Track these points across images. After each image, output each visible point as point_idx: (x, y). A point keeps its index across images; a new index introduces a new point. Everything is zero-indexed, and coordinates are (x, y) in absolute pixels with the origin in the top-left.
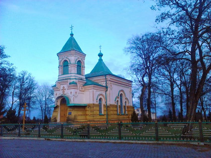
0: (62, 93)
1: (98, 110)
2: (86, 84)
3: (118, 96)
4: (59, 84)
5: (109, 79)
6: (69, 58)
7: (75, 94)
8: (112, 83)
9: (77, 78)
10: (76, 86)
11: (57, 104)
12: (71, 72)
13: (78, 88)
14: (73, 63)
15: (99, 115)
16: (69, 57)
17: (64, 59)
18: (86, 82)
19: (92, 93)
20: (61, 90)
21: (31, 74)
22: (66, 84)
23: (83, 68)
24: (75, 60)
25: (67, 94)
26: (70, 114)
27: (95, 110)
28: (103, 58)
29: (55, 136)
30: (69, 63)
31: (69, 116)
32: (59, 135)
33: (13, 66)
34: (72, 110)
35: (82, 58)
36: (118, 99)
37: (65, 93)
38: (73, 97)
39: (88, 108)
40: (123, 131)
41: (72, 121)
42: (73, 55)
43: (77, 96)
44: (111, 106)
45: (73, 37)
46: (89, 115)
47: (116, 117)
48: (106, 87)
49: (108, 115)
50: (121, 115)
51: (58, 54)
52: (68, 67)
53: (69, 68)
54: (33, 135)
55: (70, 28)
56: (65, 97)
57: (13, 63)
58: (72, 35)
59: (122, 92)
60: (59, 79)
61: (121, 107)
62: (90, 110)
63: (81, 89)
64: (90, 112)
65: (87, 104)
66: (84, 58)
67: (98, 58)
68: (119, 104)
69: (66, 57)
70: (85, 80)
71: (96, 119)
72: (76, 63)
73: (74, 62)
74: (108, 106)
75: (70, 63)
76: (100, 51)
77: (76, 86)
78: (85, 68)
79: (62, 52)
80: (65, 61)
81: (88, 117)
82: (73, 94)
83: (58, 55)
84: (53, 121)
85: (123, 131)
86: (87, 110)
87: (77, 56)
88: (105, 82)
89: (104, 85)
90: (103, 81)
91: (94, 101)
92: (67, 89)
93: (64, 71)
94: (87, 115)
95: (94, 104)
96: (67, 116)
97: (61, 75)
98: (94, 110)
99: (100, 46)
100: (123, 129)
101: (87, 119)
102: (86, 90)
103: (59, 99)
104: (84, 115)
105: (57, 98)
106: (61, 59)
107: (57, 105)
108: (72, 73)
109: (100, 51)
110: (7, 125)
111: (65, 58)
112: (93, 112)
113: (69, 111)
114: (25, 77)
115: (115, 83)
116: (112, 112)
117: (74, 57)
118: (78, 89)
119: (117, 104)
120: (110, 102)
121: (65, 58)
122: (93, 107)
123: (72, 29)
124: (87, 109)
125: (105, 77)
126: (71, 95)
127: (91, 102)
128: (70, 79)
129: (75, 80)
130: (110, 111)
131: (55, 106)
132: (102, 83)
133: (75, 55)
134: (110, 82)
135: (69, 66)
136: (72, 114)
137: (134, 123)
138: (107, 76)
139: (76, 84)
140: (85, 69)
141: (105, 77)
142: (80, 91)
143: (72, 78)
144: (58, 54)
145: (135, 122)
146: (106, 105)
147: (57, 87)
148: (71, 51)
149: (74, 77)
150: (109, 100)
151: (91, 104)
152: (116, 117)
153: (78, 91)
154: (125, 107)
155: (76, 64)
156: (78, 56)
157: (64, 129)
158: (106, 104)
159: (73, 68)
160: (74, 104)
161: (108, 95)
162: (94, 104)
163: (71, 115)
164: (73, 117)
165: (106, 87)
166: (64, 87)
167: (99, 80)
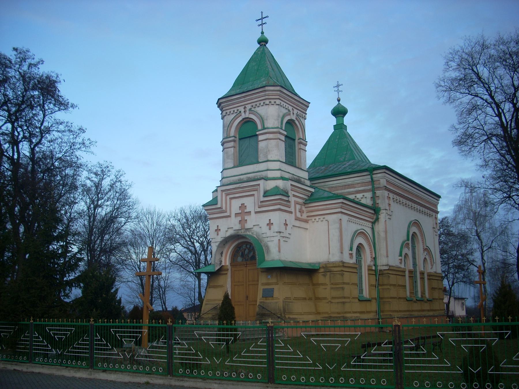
0: (238, 227)
1: (356, 284)
2: (311, 199)
3: (406, 238)
4: (227, 195)
5: (383, 182)
6: (262, 110)
7: (283, 229)
8: (391, 195)
9: (287, 176)
10: (285, 203)
11: (221, 262)
12: (266, 155)
13: (292, 209)
14: (273, 128)
15: (357, 300)
16: (261, 108)
17: (243, 116)
18: (313, 190)
19: (337, 225)
20: (233, 215)
21: (121, 173)
22: (253, 195)
23: (302, 146)
24: (279, 116)
25: (256, 229)
26: (268, 294)
27: (348, 284)
28: (347, 120)
29: (144, 367)
30: (260, 127)
32: (255, 371)
33: (82, 135)
34: (274, 280)
37: (248, 225)
38: (276, 240)
39: (325, 276)
40: (282, 353)
41: (279, 317)
42: (273, 101)
43: (288, 236)
44: (393, 271)
45: (266, 49)
46: (325, 298)
47: (403, 306)
48: (375, 210)
49: (380, 300)
50: (415, 302)
51: (221, 101)
52: (257, 142)
53: (261, 145)
54: (207, 370)
58: (263, 42)
60: (225, 181)
64: (332, 288)
65: (319, 263)
66: (304, 115)
67: (333, 121)
69: (249, 107)
70: (308, 183)
71: (350, 312)
72: (284, 128)
73: (276, 122)
74: (380, 270)
75: (264, 128)
76: (339, 100)
78: (306, 145)
79: (233, 93)
80: (247, 121)
81: (325, 307)
82: (275, 228)
83: (219, 104)
84: (210, 316)
85: (282, 353)
86: (319, 284)
87: (285, 104)
88: (369, 195)
89: (368, 201)
91: (344, 252)
92: (256, 212)
93: (240, 156)
94: (318, 299)
95: (343, 263)
97: (232, 166)
98: (344, 283)
99: (338, 86)
100: (281, 348)
101: (319, 313)
102: (313, 218)
103: (227, 247)
104: (310, 299)
105: (221, 242)
106: (232, 116)
107: (221, 263)
108: (270, 159)
109: (339, 100)
110: (116, 327)
111: (245, 112)
112: (343, 289)
113: (263, 284)
114: (106, 183)
115: (398, 198)
116: (393, 292)
117: (278, 106)
118: (291, 212)
120: (387, 256)
121: (245, 112)
122: (342, 275)
123: (262, 24)
124: (320, 278)
125: (369, 177)
126: (269, 233)
127: (335, 258)
128: (266, 179)
129: (280, 184)
130: (389, 287)
131: (217, 268)
132: (359, 196)
133: (278, 102)
134: (386, 193)
135: (260, 138)
136: (276, 294)
138: (375, 172)
139: (286, 194)
140: (307, 148)
141: (369, 177)
142: (297, 219)
143: (270, 174)
144: (221, 101)
145: (512, 320)
146: (374, 268)
147: (219, 206)
148: (267, 88)
149: (278, 174)
150: (383, 252)
151: (333, 263)
152: (403, 306)
153: (290, 219)
154: (422, 273)
155: (282, 129)
156: (287, 105)
157: (278, 348)
158: (375, 265)
159: (273, 142)
160: (282, 261)
161: (382, 235)
162: (345, 265)
163: (273, 297)
164: (281, 305)
165: (374, 210)
166: (243, 206)
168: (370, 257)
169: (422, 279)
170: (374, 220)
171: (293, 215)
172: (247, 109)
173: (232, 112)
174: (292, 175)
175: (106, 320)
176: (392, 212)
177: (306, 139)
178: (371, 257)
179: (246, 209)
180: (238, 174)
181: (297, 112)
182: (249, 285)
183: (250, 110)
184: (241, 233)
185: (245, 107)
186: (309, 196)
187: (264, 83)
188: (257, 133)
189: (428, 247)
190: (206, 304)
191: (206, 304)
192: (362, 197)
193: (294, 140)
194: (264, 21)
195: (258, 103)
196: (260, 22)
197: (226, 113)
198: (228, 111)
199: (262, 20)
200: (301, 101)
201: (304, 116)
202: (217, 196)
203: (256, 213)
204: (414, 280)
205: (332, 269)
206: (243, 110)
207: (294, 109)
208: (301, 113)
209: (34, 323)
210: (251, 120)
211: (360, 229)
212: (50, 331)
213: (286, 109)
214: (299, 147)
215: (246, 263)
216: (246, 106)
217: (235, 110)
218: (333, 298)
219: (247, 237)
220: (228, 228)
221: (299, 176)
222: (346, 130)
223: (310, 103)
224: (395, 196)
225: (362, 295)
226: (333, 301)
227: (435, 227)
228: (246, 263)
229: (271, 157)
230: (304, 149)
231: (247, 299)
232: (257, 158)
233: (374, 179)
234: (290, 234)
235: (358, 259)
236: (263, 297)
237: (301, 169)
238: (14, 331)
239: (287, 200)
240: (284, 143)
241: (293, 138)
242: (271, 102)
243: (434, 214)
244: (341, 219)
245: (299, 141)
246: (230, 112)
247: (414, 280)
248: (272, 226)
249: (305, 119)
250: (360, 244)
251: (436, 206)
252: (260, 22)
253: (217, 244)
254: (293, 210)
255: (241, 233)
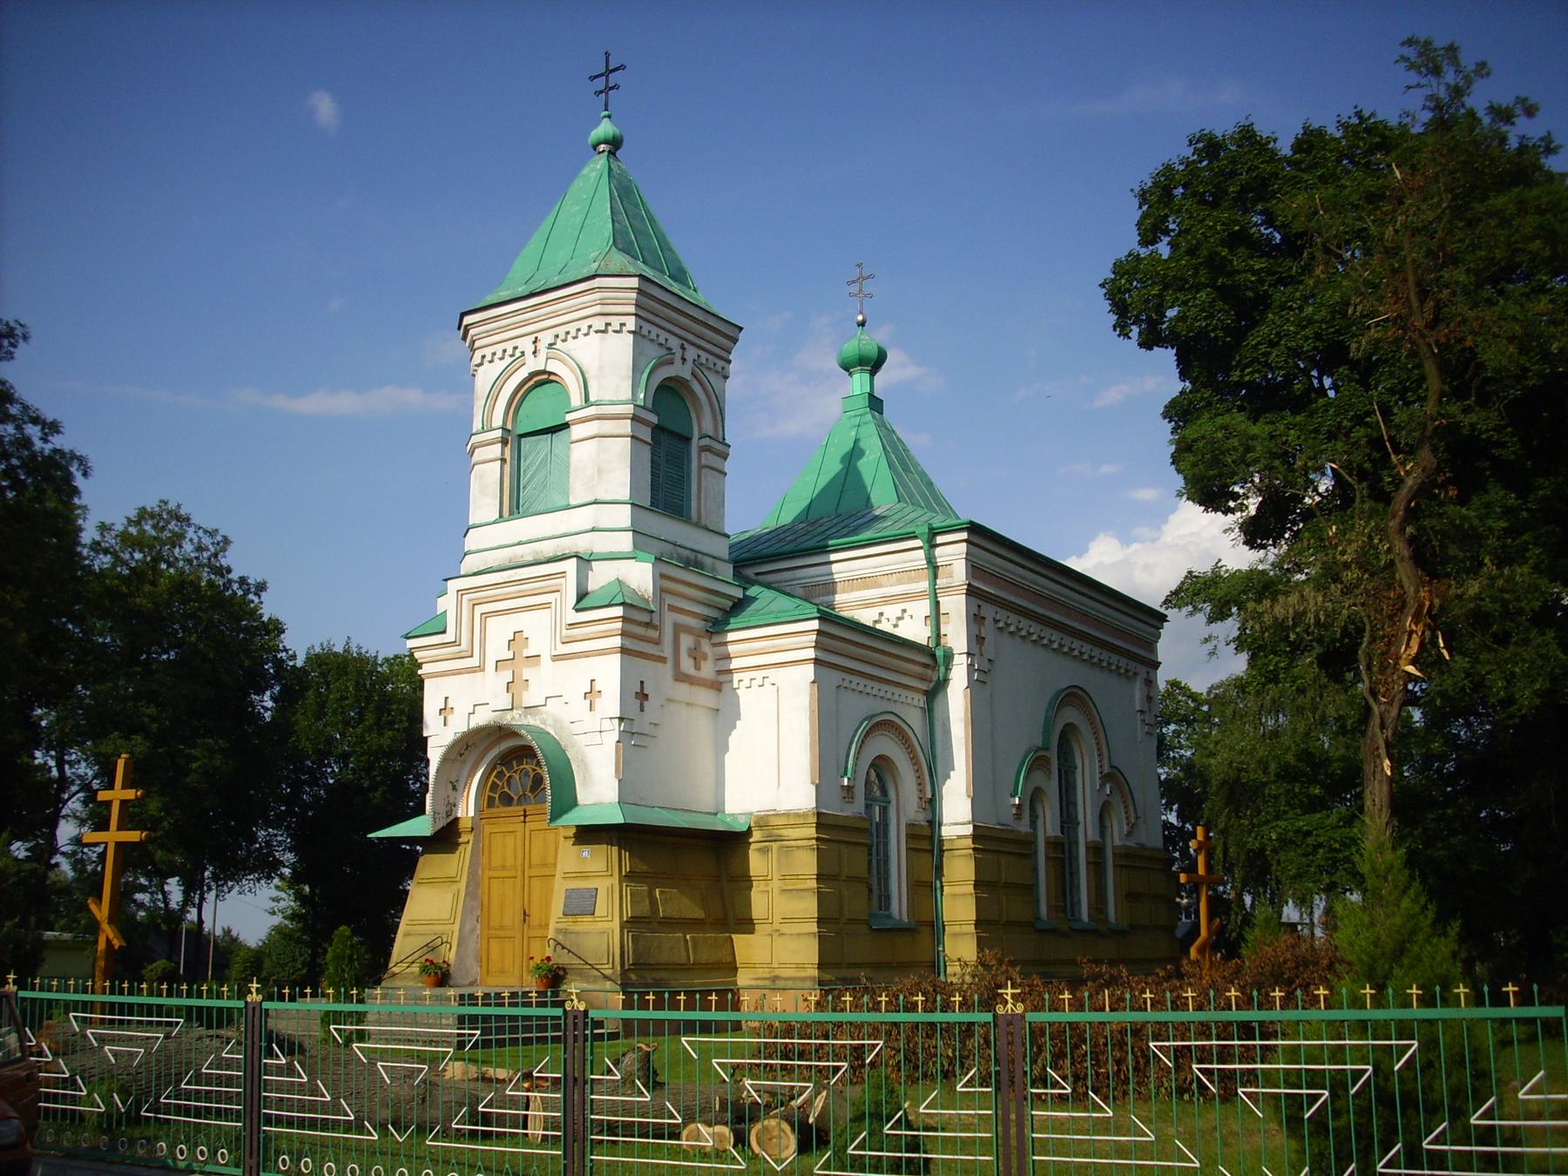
17: (533, 365)
20: (490, 665)
22: (546, 606)
30: (576, 399)
31: (568, 923)
35: (704, 355)
36: (1039, 779)
55: (593, 78)
56: (530, 739)
57: (108, 522)
59: (1071, 715)
61: (1062, 850)
62: (784, 878)
63: (691, 662)
66: (720, 363)
68: (1049, 825)
69: (546, 338)
77: (648, 625)
78: (725, 457)
87: (655, 330)
90: (907, 597)
92: (556, 658)
96: (552, 926)
106: (499, 366)
118: (663, 660)
119: (1033, 823)
132: (892, 611)
137: (1190, 1015)
138: (940, 539)
140: (728, 466)
141: (921, 553)
147: (449, 636)
166: (516, 639)
167: (867, 587)
168: (916, 799)
169: (1097, 865)
170: (932, 685)
171: (669, 666)
172: (542, 346)
173: (499, 354)
174: (671, 546)
175: (165, 986)
176: (990, 660)
177: (724, 439)
178: (921, 798)
179: (527, 647)
180: (510, 542)
181: (699, 356)
182: (530, 877)
183: (551, 346)
184: (513, 718)
185: (536, 338)
186: (725, 611)
187: (595, 265)
188: (569, 417)
189: (1117, 769)
190: (407, 935)
191: (407, 935)
192: (900, 615)
193: (687, 440)
194: (614, 78)
195: (572, 328)
196: (600, 84)
197: (484, 357)
198: (488, 352)
199: (607, 76)
200: (712, 322)
201: (723, 368)
202: (446, 611)
203: (556, 658)
204: (1067, 870)
205: (786, 832)
206: (529, 349)
207: (686, 345)
208: (710, 357)
209: (22, 994)
210: (552, 377)
211: (882, 713)
212: (83, 1029)
213: (661, 345)
214: (703, 462)
215: (525, 811)
216: (539, 335)
217: (509, 346)
218: (786, 920)
219: (523, 732)
220: (475, 706)
221: (694, 547)
222: (882, 413)
223: (741, 329)
224: (1002, 614)
225: (886, 913)
226: (786, 929)
227: (1146, 709)
228: (525, 811)
229: (606, 491)
230: (720, 468)
231: (525, 921)
232: (566, 492)
233: (940, 561)
234: (655, 725)
235: (1066, 825)
236: (565, 914)
237: (706, 528)
238: (165, 1038)
239: (648, 621)
240: (649, 447)
241: (681, 431)
242: (610, 324)
243: (1142, 670)
244: (592, 681)
245: (706, 441)
246: (494, 354)
247: (1067, 870)
248: (597, 702)
249: (726, 377)
250: (881, 758)
251: (1151, 645)
252: (600, 84)
253: (443, 750)
254: (667, 651)
255: (513, 718)
